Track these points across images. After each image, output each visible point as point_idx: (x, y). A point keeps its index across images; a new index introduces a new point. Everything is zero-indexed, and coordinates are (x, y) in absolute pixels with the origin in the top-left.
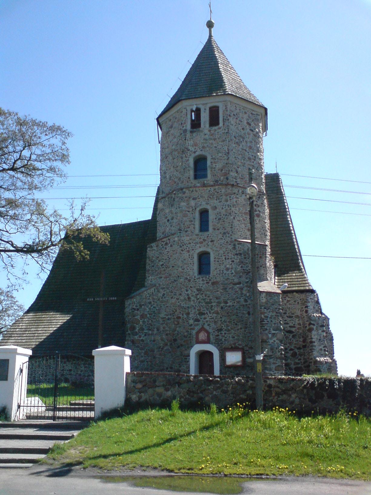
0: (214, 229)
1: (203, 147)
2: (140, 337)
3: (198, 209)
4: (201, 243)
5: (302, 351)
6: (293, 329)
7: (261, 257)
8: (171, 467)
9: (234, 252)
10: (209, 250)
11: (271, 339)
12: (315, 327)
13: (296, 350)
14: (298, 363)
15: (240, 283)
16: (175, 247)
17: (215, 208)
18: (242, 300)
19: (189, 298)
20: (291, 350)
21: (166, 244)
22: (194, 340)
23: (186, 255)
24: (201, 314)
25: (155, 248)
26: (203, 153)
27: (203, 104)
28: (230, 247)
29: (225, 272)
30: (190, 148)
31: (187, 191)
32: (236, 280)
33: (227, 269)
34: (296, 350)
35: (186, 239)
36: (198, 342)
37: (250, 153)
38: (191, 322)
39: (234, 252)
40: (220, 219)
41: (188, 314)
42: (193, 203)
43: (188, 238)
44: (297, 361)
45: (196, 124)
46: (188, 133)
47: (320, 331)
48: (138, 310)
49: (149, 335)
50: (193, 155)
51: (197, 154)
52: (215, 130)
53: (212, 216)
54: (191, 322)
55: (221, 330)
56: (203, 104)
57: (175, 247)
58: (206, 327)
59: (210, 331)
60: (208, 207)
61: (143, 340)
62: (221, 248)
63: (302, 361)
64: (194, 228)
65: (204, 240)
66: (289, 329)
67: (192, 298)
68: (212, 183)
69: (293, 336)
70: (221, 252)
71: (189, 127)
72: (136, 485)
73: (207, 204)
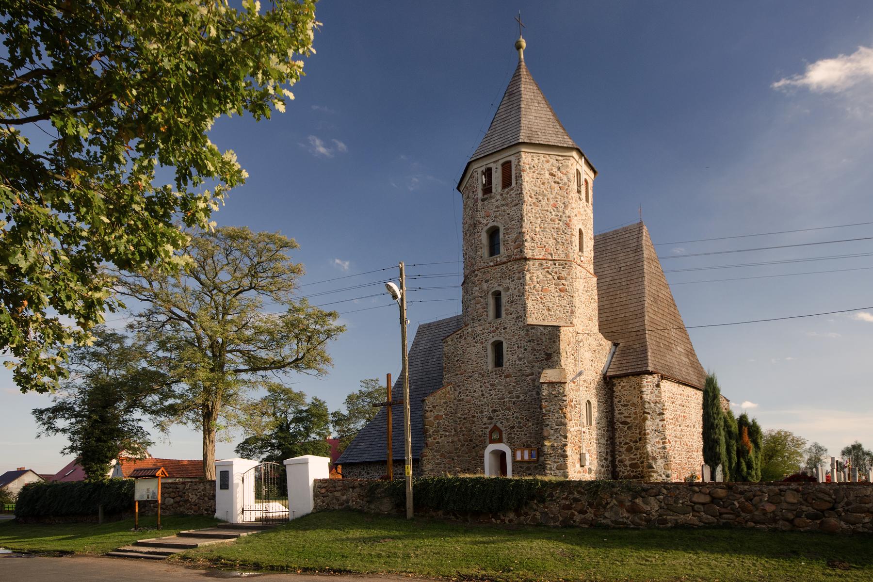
0: (507, 314)
1: (495, 217)
2: (435, 439)
3: (490, 293)
4: (494, 332)
5: (638, 444)
6: (628, 420)
7: (554, 342)
8: (233, 558)
9: (527, 338)
10: (502, 339)
11: (553, 435)
12: (649, 416)
13: (632, 444)
14: (634, 459)
15: (532, 374)
16: (469, 339)
17: (508, 289)
18: (534, 393)
19: (483, 395)
20: (626, 443)
21: (461, 337)
22: (488, 441)
23: (479, 347)
24: (495, 411)
25: (450, 343)
26: (495, 224)
27: (494, 162)
28: (523, 333)
29: (517, 362)
30: (481, 220)
31: (479, 274)
32: (528, 371)
33: (520, 359)
34: (632, 444)
35: (478, 329)
36: (492, 441)
37: (553, 213)
38: (485, 420)
39: (527, 338)
40: (512, 302)
41: (482, 412)
42: (485, 286)
43: (481, 328)
44: (632, 456)
45: (487, 189)
46: (479, 201)
47: (658, 420)
48: (431, 411)
49: (445, 436)
50: (486, 228)
51: (489, 226)
52: (508, 193)
53: (504, 299)
54: (485, 420)
55: (513, 427)
56: (494, 162)
57: (469, 339)
58: (499, 425)
59: (502, 429)
60: (500, 289)
61: (438, 443)
62: (513, 336)
63: (638, 456)
64: (487, 315)
65: (497, 328)
66: (624, 419)
67: (486, 395)
68: (505, 260)
69: (628, 428)
70: (514, 340)
71: (480, 194)
72: (28, 557)
73: (499, 285)
